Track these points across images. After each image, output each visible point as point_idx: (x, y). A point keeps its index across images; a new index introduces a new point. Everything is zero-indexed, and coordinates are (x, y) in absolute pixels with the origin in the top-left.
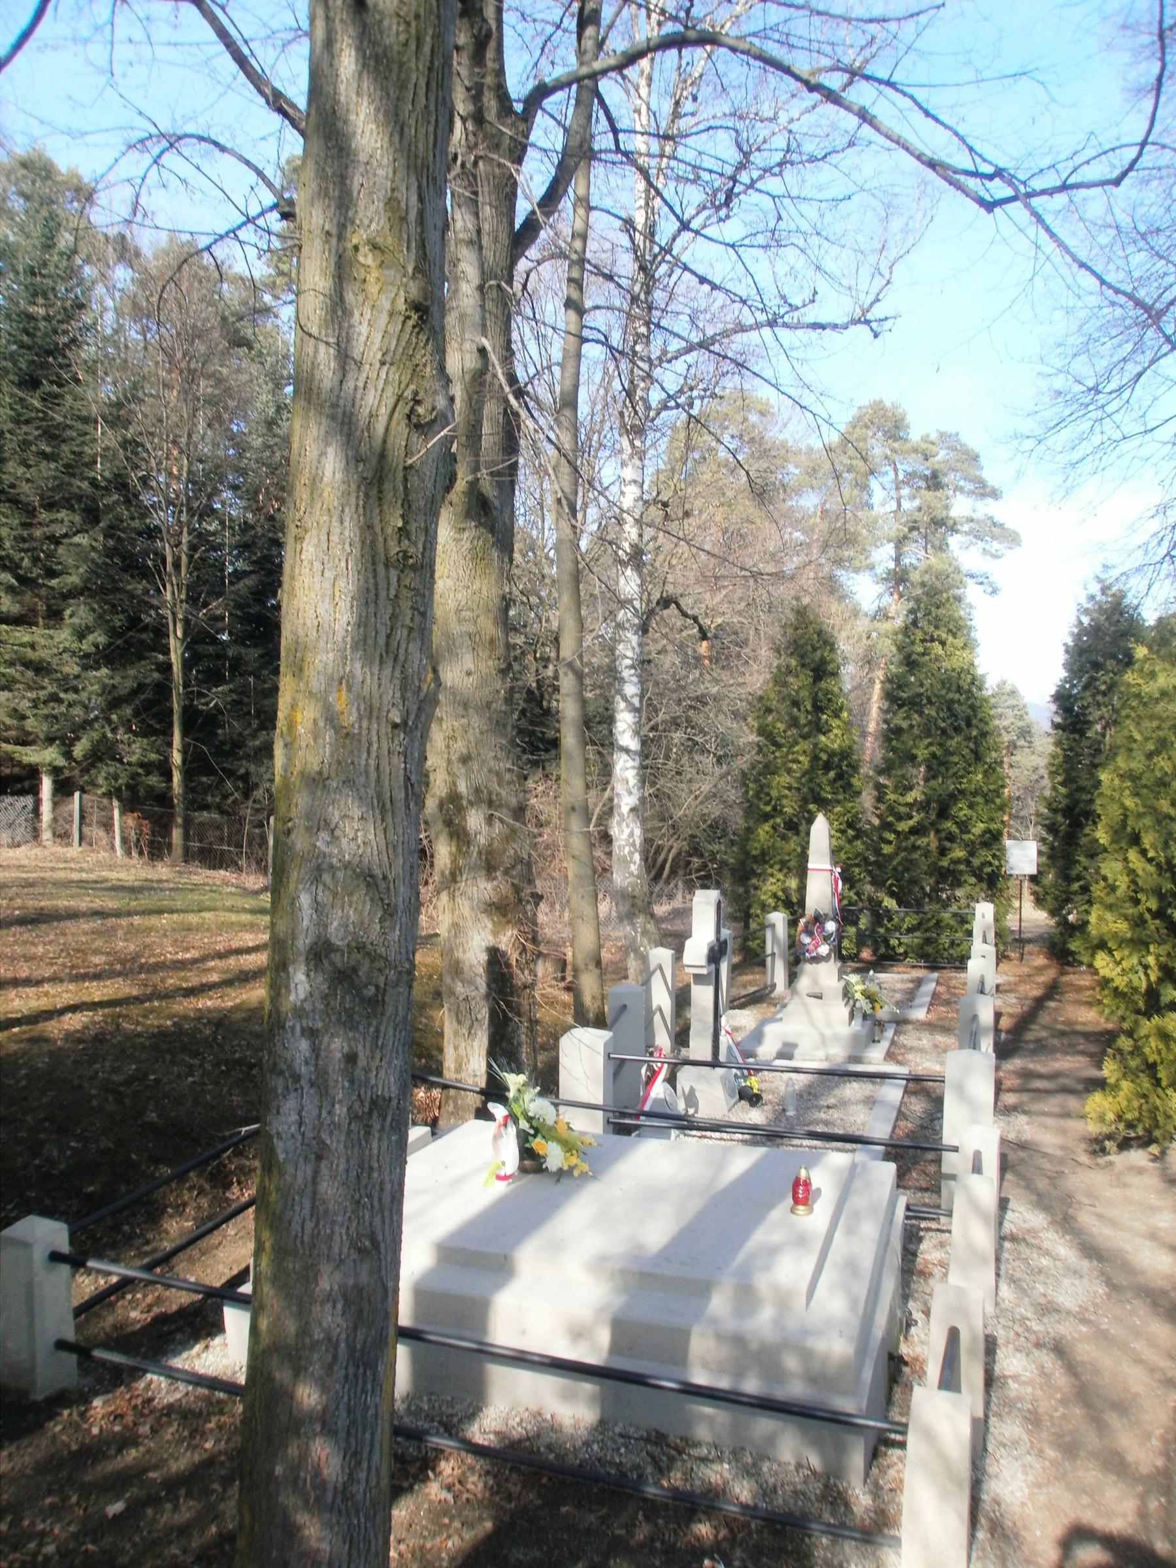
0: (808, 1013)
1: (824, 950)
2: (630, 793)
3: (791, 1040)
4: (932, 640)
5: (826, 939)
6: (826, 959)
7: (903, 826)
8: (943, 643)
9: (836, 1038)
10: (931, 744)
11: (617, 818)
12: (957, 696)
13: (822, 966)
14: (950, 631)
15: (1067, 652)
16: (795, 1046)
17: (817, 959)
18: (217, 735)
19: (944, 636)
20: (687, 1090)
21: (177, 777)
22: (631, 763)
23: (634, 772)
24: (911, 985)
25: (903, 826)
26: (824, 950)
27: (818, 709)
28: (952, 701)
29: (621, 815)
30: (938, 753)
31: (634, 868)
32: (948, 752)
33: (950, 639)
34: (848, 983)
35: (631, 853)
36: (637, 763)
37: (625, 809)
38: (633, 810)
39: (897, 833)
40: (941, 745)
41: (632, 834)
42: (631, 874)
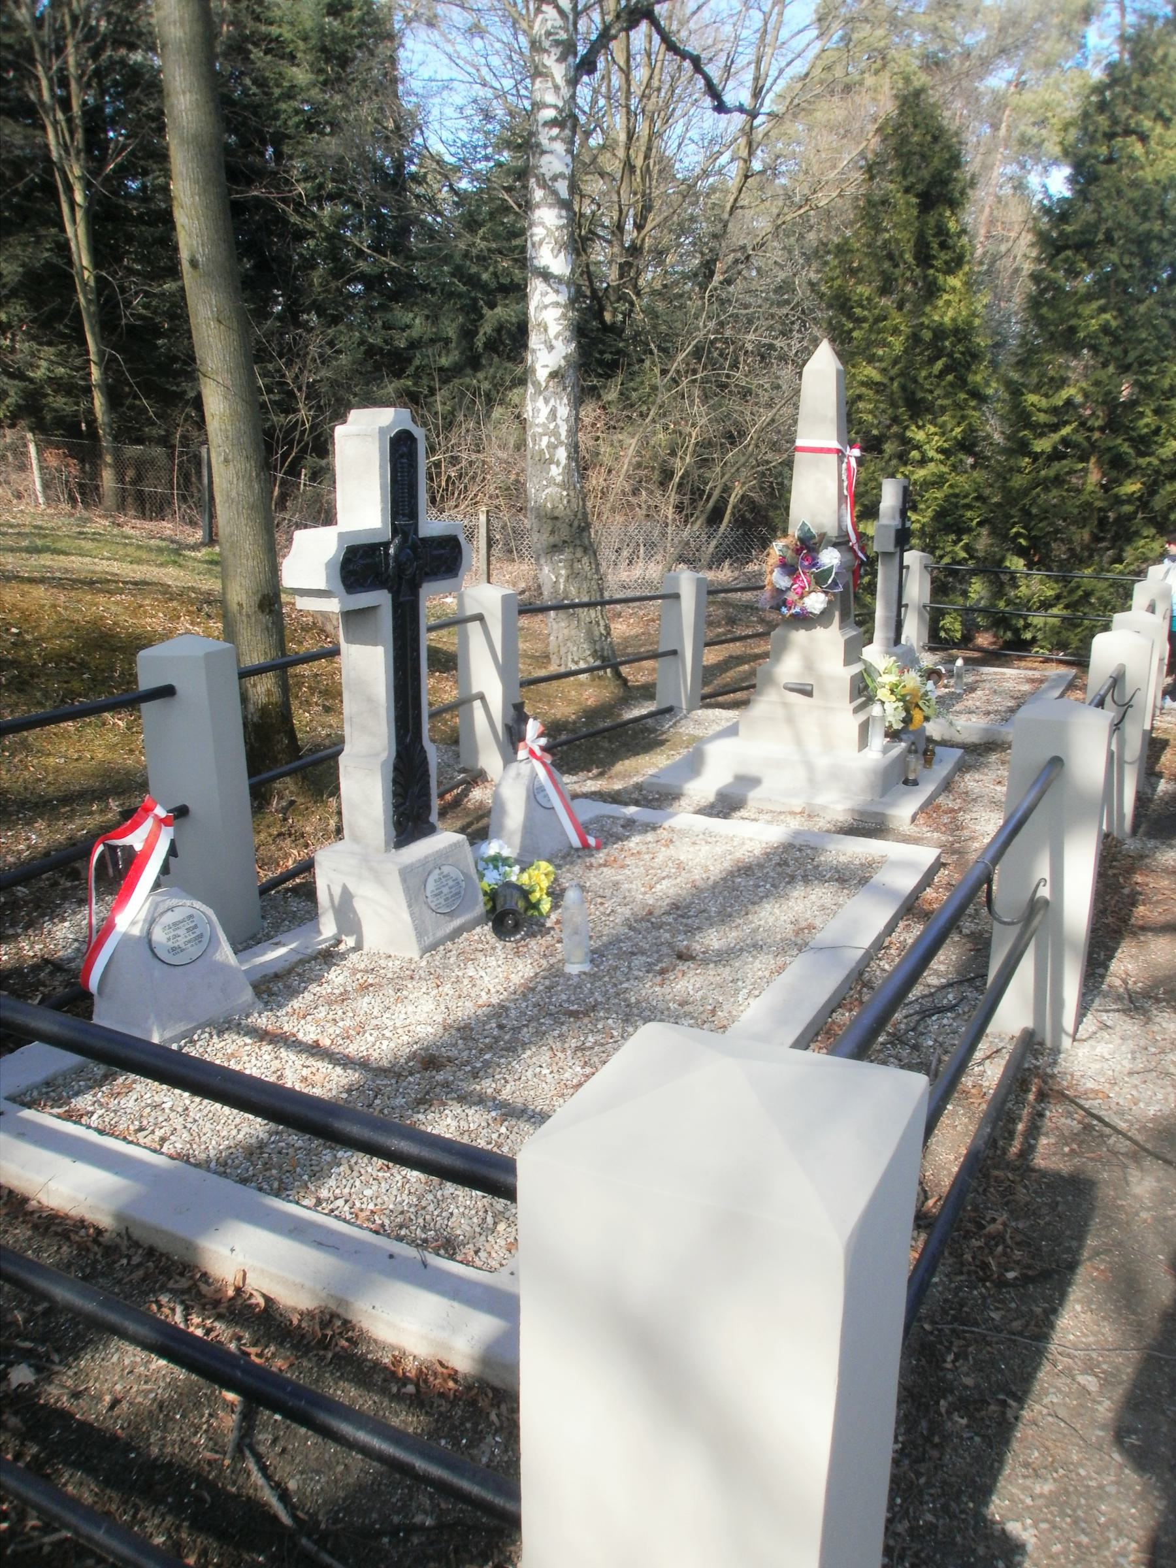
0: (790, 720)
1: (816, 602)
2: (551, 348)
3: (752, 770)
4: (1128, 132)
5: (820, 579)
6: (823, 618)
7: (1042, 445)
8: (1143, 138)
9: (836, 775)
10: (1102, 310)
11: (531, 389)
12: (1157, 226)
13: (819, 632)
14: (1160, 116)
15: (922, 1220)
16: (754, 782)
17: (805, 620)
18: (156, 347)
19: (1147, 124)
20: (337, 891)
21: (99, 401)
22: (552, 297)
23: (558, 312)
24: (1026, 687)
25: (1042, 445)
26: (816, 602)
27: (924, 258)
28: (1149, 236)
29: (536, 384)
30: (1114, 324)
31: (555, 472)
32: (1130, 325)
33: (1159, 129)
34: (869, 670)
35: (552, 447)
36: (562, 298)
37: (542, 374)
38: (553, 375)
39: (1035, 457)
40: (1121, 312)
41: (553, 413)
42: (551, 482)
